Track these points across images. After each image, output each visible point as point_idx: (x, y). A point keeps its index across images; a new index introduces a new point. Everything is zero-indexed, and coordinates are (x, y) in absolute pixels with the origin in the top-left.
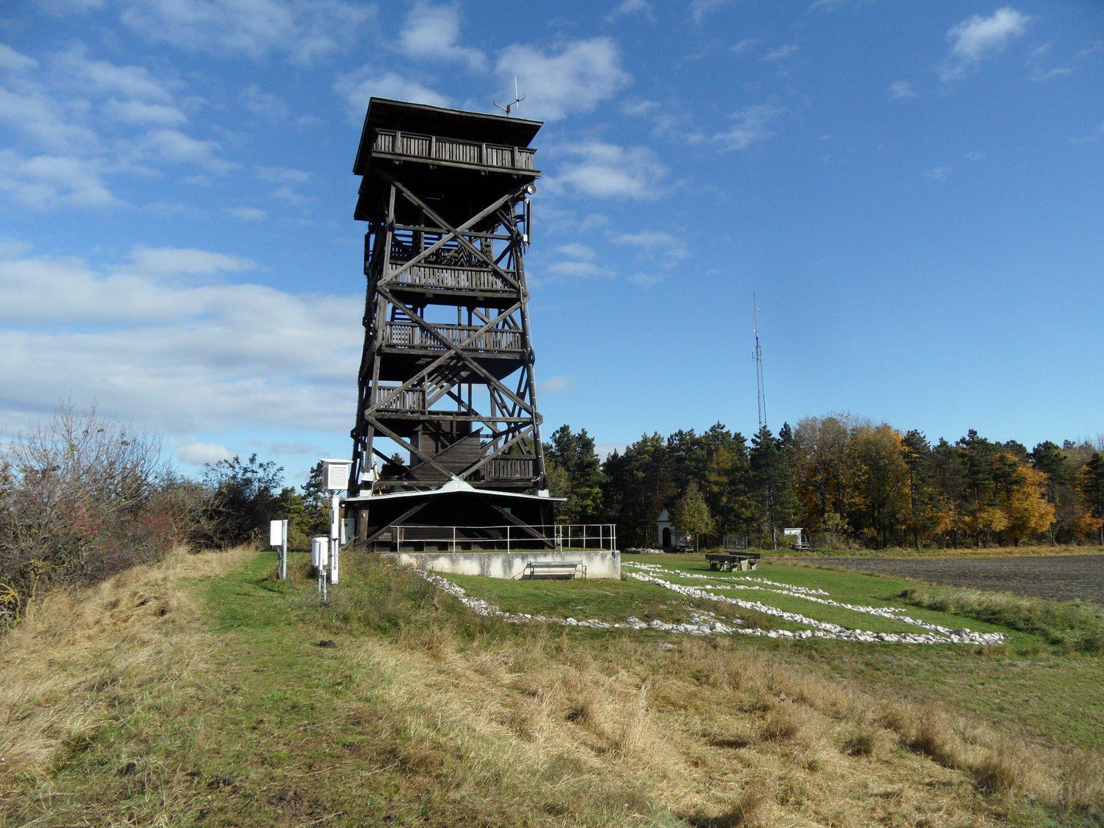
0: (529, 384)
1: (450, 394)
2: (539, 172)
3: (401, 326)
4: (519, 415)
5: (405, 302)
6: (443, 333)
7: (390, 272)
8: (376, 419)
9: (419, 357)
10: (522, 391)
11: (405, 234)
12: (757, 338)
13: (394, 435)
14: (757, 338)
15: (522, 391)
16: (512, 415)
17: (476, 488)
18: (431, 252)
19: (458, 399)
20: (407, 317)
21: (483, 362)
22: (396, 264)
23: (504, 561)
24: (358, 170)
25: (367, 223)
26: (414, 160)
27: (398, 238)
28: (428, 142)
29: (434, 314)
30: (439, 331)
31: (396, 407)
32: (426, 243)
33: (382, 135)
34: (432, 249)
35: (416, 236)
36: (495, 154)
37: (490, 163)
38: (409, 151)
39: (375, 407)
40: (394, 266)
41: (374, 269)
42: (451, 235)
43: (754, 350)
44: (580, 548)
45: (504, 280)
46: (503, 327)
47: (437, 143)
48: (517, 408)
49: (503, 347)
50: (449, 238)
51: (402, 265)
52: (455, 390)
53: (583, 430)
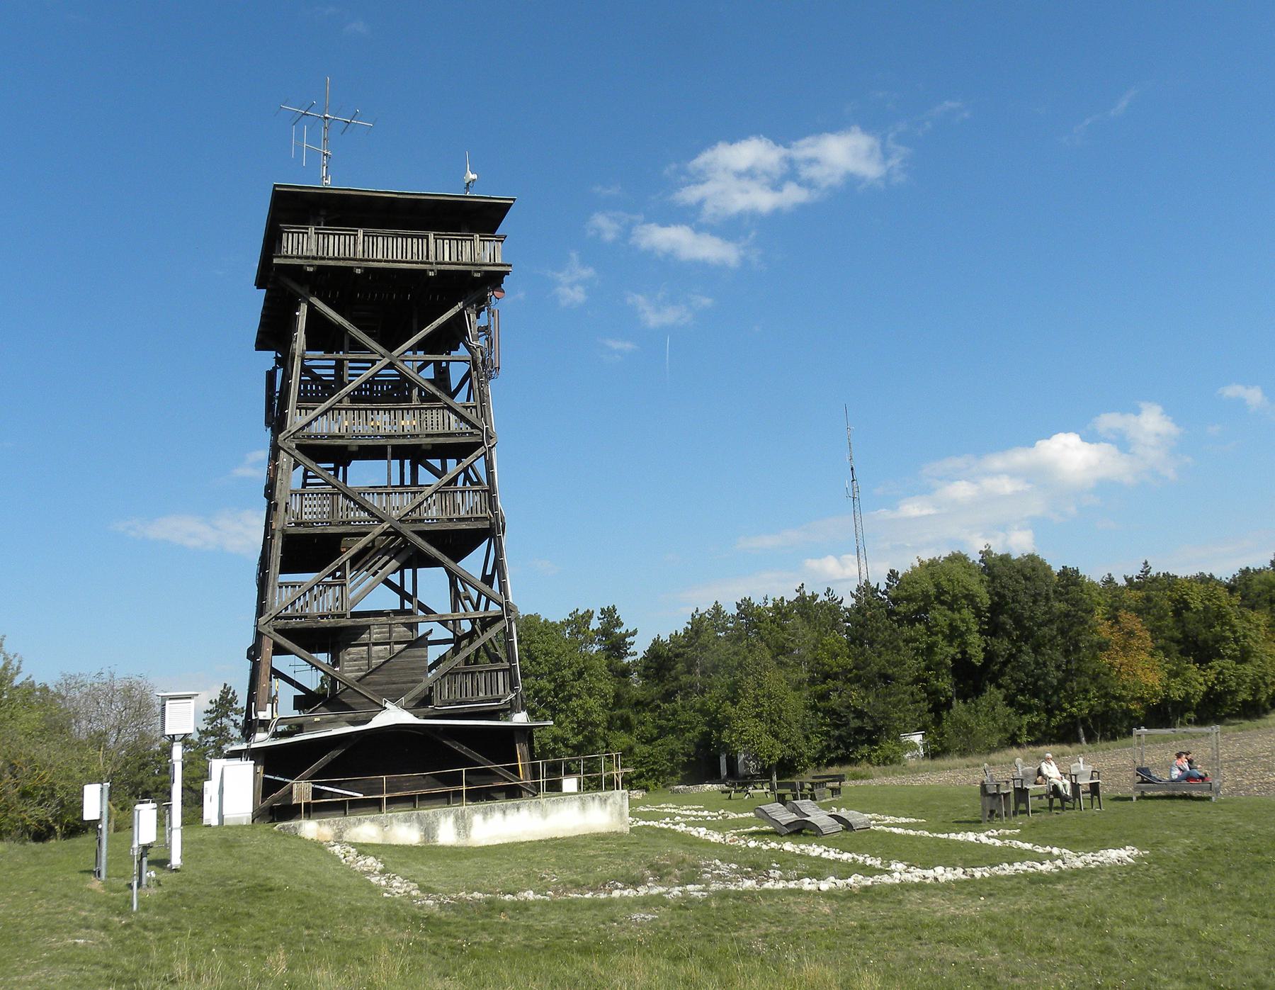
0: (499, 566)
1: (388, 583)
2: (511, 266)
3: (313, 494)
4: (486, 608)
5: (318, 461)
6: (374, 501)
7: (296, 419)
8: (275, 630)
9: (341, 536)
10: (489, 572)
11: (323, 363)
12: (852, 469)
13: (304, 653)
14: (852, 469)
15: (489, 572)
16: (476, 608)
17: (426, 718)
18: (364, 379)
19: (399, 590)
20: (320, 481)
21: (428, 536)
22: (306, 409)
23: (457, 818)
24: (260, 284)
25: (273, 353)
26: (331, 263)
27: (316, 371)
28: (352, 237)
29: (362, 474)
30: (367, 497)
31: (318, 610)
32: (350, 375)
33: (288, 233)
34: (357, 381)
35: (339, 365)
36: (447, 247)
37: (440, 259)
38: (325, 252)
39: (274, 613)
40: (303, 411)
41: (276, 420)
42: (386, 361)
43: (848, 483)
44: (556, 793)
45: (462, 418)
46: (464, 484)
47: (366, 238)
48: (484, 599)
49: (463, 514)
50: (382, 366)
51: (314, 409)
52: (395, 578)
53: (1110, 575)
